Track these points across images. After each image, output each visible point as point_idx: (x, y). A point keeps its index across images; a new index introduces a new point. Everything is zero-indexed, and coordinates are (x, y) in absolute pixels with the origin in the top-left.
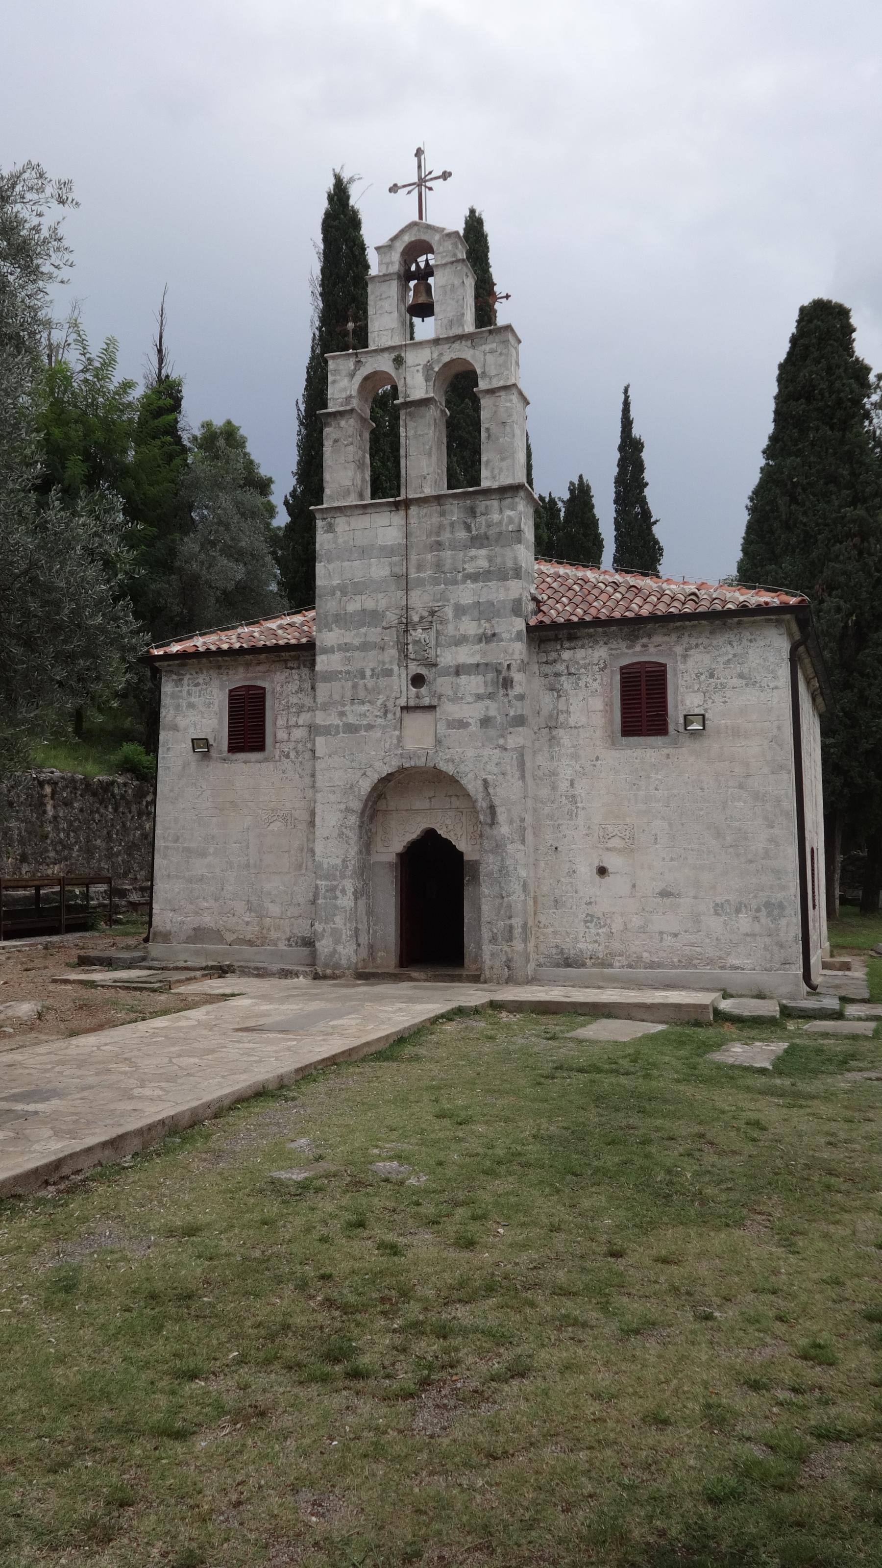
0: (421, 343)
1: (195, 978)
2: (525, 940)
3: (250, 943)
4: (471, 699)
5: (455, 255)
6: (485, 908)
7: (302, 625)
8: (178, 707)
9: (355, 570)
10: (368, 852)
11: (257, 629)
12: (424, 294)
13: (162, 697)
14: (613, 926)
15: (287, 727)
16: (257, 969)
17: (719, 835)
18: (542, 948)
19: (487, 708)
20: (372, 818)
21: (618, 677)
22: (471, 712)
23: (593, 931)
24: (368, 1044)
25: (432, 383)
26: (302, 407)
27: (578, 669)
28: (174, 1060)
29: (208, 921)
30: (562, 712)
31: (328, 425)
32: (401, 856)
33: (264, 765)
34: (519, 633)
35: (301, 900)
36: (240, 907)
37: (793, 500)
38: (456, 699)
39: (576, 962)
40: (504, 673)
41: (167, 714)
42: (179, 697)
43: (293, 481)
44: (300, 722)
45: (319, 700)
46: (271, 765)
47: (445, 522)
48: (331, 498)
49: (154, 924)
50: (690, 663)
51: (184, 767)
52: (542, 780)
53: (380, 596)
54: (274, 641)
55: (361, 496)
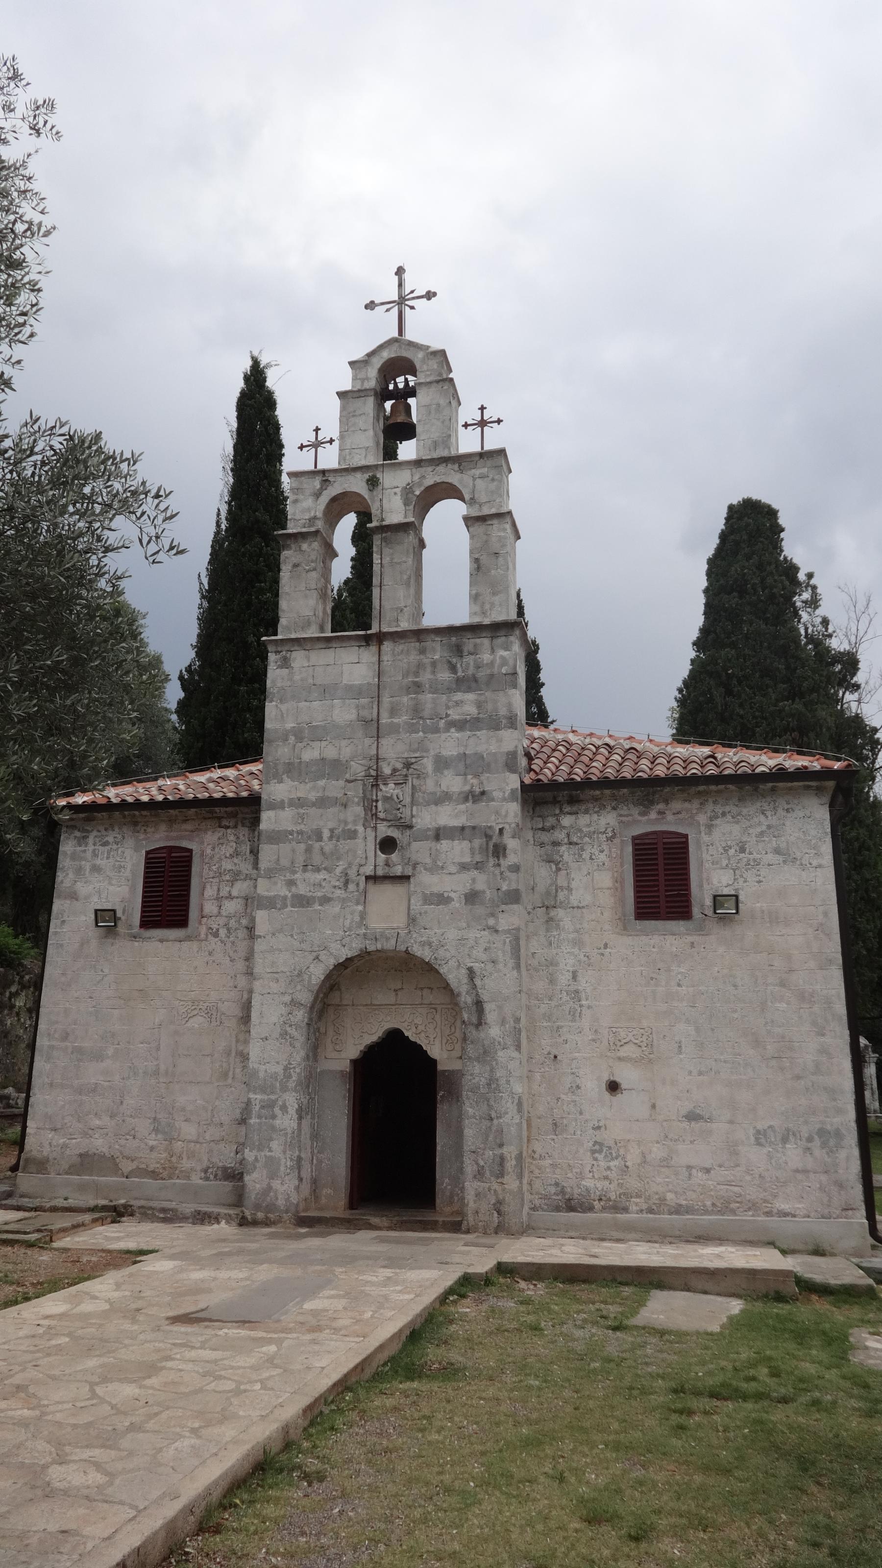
0: (402, 464)
1: (83, 1225)
2: (520, 1176)
3: (154, 1175)
4: (453, 869)
5: (440, 374)
6: (469, 1132)
7: (238, 778)
8: (79, 871)
9: (315, 711)
10: (316, 1059)
11: (181, 782)
12: (403, 414)
13: (60, 857)
14: (629, 1157)
15: (217, 899)
16: (164, 1210)
17: (757, 1043)
18: (537, 1185)
19: (474, 880)
20: (321, 1014)
21: (629, 849)
22: (454, 885)
23: (602, 1164)
24: (381, 1348)
25: (411, 507)
26: (205, 581)
27: (581, 838)
28: (99, 1390)
29: (99, 1144)
30: (562, 888)
31: (287, 547)
32: (354, 1062)
33: (186, 945)
34: (513, 791)
35: (225, 1119)
36: (143, 1126)
37: (729, 692)
38: (435, 868)
39: (581, 1204)
40: (495, 839)
41: (65, 878)
42: (82, 859)
43: (192, 654)
44: (235, 893)
45: (263, 865)
46: (195, 945)
47: (426, 661)
48: (288, 629)
49: (27, 1147)
50: (717, 834)
51: (82, 945)
52: (537, 970)
53: (344, 743)
54: (207, 795)
55: (322, 629)
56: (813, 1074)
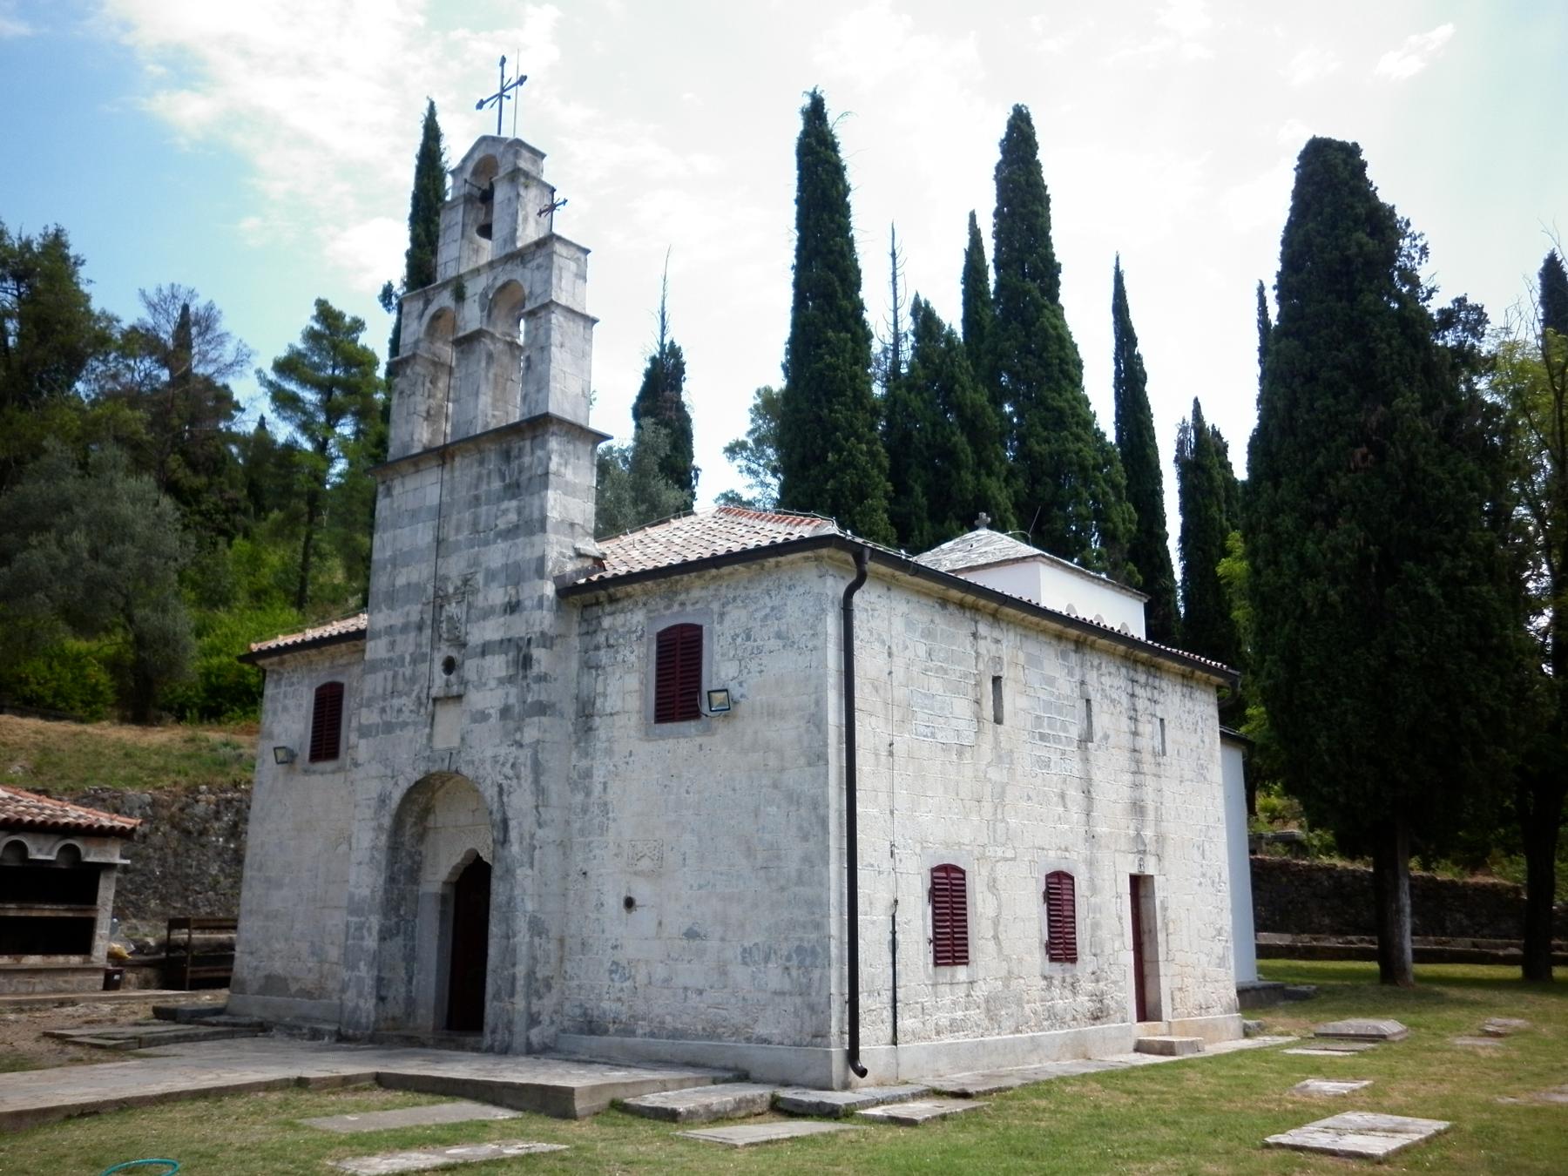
4: (493, 684)
17: (750, 852)
29: (278, 967)
50: (727, 622)
56: (796, 884)
